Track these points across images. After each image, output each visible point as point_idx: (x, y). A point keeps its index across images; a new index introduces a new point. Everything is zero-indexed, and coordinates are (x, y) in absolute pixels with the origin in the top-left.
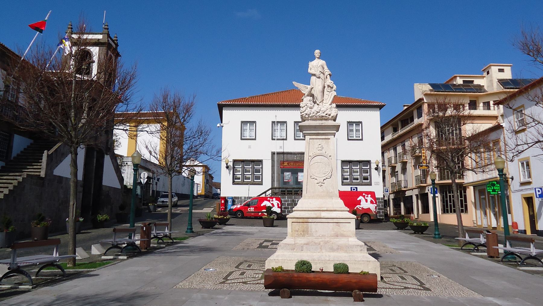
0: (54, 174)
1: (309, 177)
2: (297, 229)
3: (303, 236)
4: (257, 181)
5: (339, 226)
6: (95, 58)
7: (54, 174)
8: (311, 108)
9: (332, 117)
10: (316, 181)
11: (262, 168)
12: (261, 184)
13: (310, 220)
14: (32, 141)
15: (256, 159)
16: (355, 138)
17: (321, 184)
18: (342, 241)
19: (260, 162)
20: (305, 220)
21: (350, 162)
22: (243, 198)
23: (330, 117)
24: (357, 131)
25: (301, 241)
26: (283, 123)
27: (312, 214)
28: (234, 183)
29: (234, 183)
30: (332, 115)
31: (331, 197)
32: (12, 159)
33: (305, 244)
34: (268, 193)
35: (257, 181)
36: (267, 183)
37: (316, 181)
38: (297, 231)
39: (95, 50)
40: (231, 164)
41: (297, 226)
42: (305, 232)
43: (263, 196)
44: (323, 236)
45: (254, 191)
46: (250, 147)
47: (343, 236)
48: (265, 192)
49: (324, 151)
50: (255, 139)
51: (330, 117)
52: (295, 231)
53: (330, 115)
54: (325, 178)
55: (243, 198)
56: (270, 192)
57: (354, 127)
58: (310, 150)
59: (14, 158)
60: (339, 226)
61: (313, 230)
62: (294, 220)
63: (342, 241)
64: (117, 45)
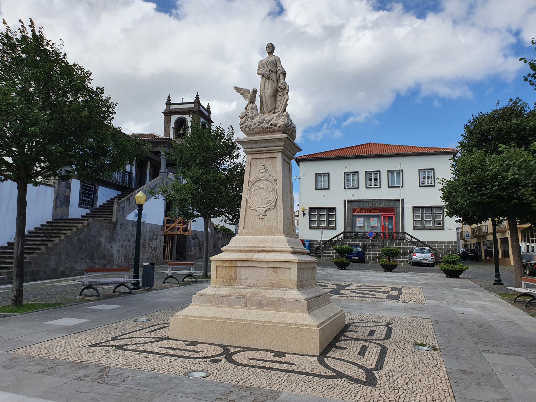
0: (127, 219)
1: (248, 208)
2: (222, 275)
3: (230, 284)
4: (331, 226)
5: (276, 272)
6: (189, 124)
7: (127, 219)
8: (252, 118)
9: (279, 127)
10: (256, 214)
11: (335, 214)
12: (335, 228)
13: (239, 264)
14: (120, 193)
15: (330, 206)
16: (427, 185)
17: (262, 217)
18: (276, 294)
19: (333, 209)
20: (232, 264)
21: (422, 208)
22: (319, 241)
23: (277, 128)
24: (430, 178)
25: (225, 291)
26: (355, 173)
27: (243, 256)
28: (310, 228)
29: (310, 228)
30: (278, 125)
31: (273, 233)
32: (98, 207)
33: (226, 296)
34: (340, 237)
35: (331, 226)
36: (341, 227)
37: (256, 214)
38: (223, 278)
39: (189, 118)
40: (307, 212)
41: (223, 272)
42: (232, 280)
43: (336, 239)
44: (254, 285)
45: (328, 235)
46: (324, 196)
47: (280, 286)
48: (337, 236)
49: (268, 174)
50: (329, 189)
51: (277, 128)
52: (220, 277)
53: (276, 125)
54: (267, 208)
55: (319, 241)
56: (342, 235)
57: (426, 174)
58: (252, 173)
59: (100, 206)
60: (276, 272)
61: (243, 277)
62: (220, 263)
63: (276, 294)
64: (210, 113)
